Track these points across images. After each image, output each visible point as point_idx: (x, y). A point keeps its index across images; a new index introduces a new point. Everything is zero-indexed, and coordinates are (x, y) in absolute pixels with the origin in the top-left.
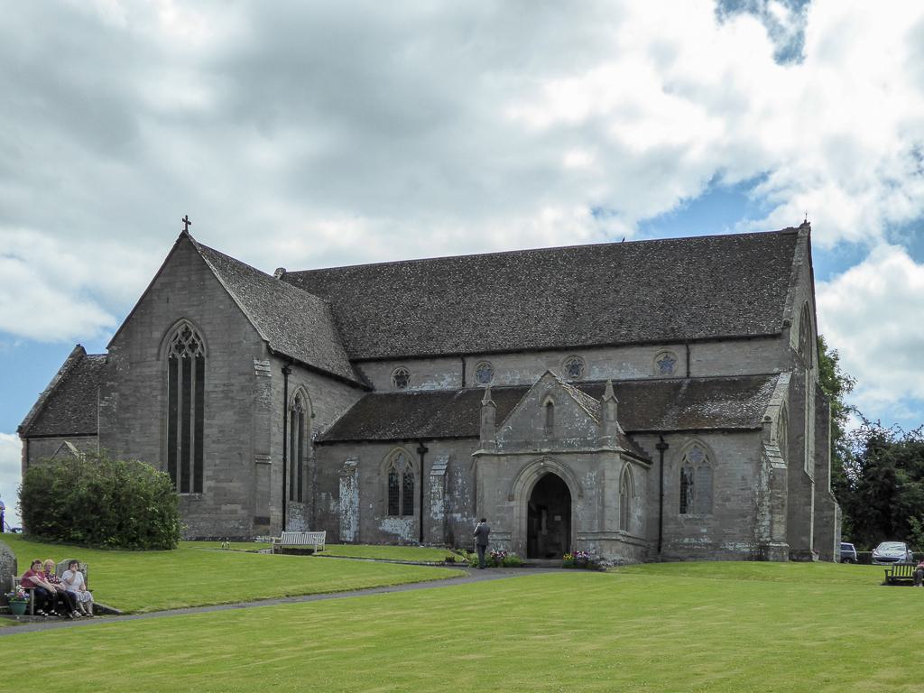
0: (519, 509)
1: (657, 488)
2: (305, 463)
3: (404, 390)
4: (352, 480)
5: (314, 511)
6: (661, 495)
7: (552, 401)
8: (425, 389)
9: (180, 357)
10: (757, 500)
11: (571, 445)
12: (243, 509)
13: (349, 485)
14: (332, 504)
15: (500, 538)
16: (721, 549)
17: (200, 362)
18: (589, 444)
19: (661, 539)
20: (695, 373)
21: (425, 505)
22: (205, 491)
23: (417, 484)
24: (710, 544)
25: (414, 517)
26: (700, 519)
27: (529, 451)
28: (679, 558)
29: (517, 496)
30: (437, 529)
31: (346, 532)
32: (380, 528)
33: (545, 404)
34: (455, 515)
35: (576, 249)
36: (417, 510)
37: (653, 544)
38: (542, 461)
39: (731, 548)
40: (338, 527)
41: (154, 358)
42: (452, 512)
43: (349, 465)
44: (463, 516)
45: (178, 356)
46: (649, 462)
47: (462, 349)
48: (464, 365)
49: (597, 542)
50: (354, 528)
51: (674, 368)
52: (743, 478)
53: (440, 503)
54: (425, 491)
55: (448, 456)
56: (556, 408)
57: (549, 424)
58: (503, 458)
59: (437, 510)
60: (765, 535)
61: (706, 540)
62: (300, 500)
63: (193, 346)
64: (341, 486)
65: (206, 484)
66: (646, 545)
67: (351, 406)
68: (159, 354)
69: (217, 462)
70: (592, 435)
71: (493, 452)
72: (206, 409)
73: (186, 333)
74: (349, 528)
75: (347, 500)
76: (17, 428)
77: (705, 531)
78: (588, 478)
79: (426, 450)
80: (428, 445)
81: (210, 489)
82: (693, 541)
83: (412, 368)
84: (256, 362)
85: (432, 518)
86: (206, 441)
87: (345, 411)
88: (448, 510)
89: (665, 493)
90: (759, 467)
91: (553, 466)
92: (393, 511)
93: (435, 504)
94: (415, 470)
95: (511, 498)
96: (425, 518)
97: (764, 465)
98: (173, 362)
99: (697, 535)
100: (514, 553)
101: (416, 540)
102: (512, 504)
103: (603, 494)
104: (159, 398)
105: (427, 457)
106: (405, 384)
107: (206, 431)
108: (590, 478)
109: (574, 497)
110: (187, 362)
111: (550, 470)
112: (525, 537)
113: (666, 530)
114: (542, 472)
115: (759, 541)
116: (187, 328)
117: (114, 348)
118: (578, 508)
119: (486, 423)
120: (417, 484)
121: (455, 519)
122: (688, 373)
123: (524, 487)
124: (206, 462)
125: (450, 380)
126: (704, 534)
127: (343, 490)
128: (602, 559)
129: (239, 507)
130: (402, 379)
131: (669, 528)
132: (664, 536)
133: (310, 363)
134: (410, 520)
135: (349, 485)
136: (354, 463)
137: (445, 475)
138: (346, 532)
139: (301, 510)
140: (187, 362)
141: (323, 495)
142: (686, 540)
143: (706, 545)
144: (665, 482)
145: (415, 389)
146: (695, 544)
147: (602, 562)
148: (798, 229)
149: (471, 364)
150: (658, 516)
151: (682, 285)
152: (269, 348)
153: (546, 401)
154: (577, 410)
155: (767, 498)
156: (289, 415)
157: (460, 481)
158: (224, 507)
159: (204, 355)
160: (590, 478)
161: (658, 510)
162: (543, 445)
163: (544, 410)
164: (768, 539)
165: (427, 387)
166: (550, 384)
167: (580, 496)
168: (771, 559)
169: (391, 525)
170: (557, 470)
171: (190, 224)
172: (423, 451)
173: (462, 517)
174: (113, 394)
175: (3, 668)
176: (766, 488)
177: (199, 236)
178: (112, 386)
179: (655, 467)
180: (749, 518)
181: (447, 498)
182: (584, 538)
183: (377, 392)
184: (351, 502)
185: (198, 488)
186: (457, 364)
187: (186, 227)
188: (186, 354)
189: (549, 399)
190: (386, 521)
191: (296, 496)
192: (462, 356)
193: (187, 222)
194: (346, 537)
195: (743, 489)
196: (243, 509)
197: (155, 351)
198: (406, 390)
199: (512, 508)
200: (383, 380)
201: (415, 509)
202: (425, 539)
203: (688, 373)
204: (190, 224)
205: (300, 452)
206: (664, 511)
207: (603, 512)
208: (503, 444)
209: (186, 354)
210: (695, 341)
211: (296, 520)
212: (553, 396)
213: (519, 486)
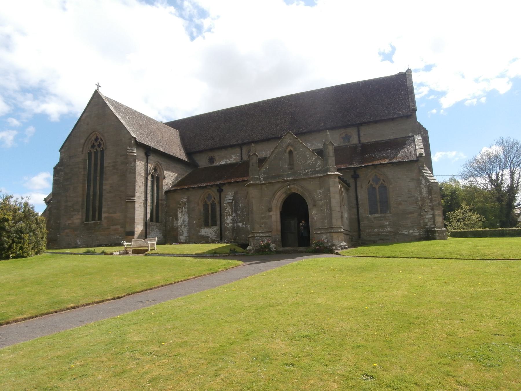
0: (275, 216)
1: (354, 202)
2: (160, 202)
3: (213, 165)
4: (184, 209)
5: (165, 227)
6: (357, 204)
7: (292, 149)
8: (223, 163)
9: (93, 151)
10: (420, 203)
11: (306, 174)
12: (121, 227)
13: (182, 212)
14: (175, 222)
15: (264, 235)
16: (400, 234)
17: (102, 152)
18: (318, 172)
19: (359, 230)
20: (363, 140)
21: (223, 219)
22: (103, 219)
23: (218, 209)
24: (392, 232)
25: (217, 227)
26: (383, 217)
27: (279, 180)
28: (372, 241)
29: (274, 209)
30: (229, 232)
31: (181, 237)
32: (200, 234)
33: (287, 151)
34: (239, 224)
35: (292, 96)
36: (218, 223)
37: (355, 234)
38: (289, 185)
39: (406, 233)
40: (177, 235)
41: (81, 153)
42: (237, 223)
43: (182, 201)
44: (243, 224)
45: (92, 151)
46: (349, 186)
47: (240, 142)
48: (241, 150)
49: (328, 234)
50: (186, 234)
51: (351, 139)
52: (409, 191)
53: (230, 218)
54: (222, 212)
55: (233, 193)
56: (295, 153)
57: (291, 164)
58: (264, 186)
59: (228, 221)
60: (429, 224)
61: (389, 229)
62: (157, 221)
63: (99, 145)
64: (178, 213)
65: (104, 215)
66: (351, 234)
67: (187, 174)
68: (83, 151)
69: (109, 203)
70: (319, 167)
71: (257, 182)
72: (104, 176)
73: (96, 139)
74: (183, 235)
75: (182, 220)
76: (44, 199)
77: (387, 223)
78: (319, 194)
79: (222, 190)
80: (224, 188)
81: (106, 218)
82: (380, 230)
83: (216, 155)
84: (128, 148)
85: (226, 227)
86: (104, 193)
87: (184, 176)
88: (234, 221)
89: (360, 203)
90: (419, 182)
91: (295, 189)
92: (207, 225)
93: (227, 219)
94: (217, 201)
95: (270, 210)
96: (223, 227)
97: (423, 182)
98: (90, 154)
99: (383, 227)
100: (274, 245)
101: (218, 239)
102: (271, 213)
103: (330, 202)
104: (82, 173)
105: (223, 195)
106: (213, 162)
107: (104, 187)
108: (320, 193)
109: (310, 206)
110: (96, 153)
111: (293, 191)
112: (280, 233)
113: (362, 224)
114: (289, 192)
115: (425, 228)
116: (97, 137)
117: (63, 150)
118: (314, 213)
119: (253, 166)
120: (218, 209)
121: (239, 226)
122: (360, 141)
123: (277, 204)
124: (104, 203)
125: (234, 158)
126: (387, 225)
127: (179, 215)
128: (334, 245)
129: (119, 227)
130: (212, 160)
131: (364, 223)
132: (361, 228)
133: (162, 150)
134: (215, 228)
135: (182, 212)
136: (185, 200)
137: (232, 202)
138: (181, 237)
139: (157, 226)
140: (96, 153)
141: (171, 218)
142: (376, 230)
143: (389, 232)
144: (359, 197)
145: (218, 164)
146: (381, 232)
147: (334, 248)
148: (405, 72)
149: (245, 149)
150: (357, 217)
151: (349, 102)
152: (136, 141)
153: (288, 149)
154: (308, 153)
155: (428, 201)
156: (149, 178)
157: (240, 205)
158: (112, 227)
159: (104, 148)
160: (320, 193)
161: (356, 213)
162: (288, 176)
163: (287, 155)
164: (433, 226)
165: (223, 162)
166: (290, 139)
167: (315, 205)
168: (437, 238)
169: (205, 231)
170: (298, 190)
171: (100, 87)
172: (220, 191)
173: (242, 225)
174: (61, 173)
175: (1, 320)
176: (426, 195)
177: (104, 93)
178: (60, 169)
179: (352, 188)
180: (416, 215)
181: (234, 215)
182: (319, 232)
183: (200, 167)
184: (184, 221)
185: (100, 218)
186: (238, 150)
187: (98, 88)
188: (96, 150)
189: (290, 148)
190: (202, 230)
191: (154, 219)
192: (240, 146)
193: (98, 86)
194: (181, 240)
195: (409, 197)
196: (121, 227)
197: (81, 149)
198: (214, 165)
199: (271, 216)
200: (203, 162)
201: (217, 222)
202: (223, 238)
203: (360, 141)
204: (100, 87)
205: (158, 196)
206: (360, 213)
207: (331, 214)
208: (264, 178)
209: (96, 150)
210: (361, 124)
211: (154, 232)
212: (292, 146)
213: (275, 202)
